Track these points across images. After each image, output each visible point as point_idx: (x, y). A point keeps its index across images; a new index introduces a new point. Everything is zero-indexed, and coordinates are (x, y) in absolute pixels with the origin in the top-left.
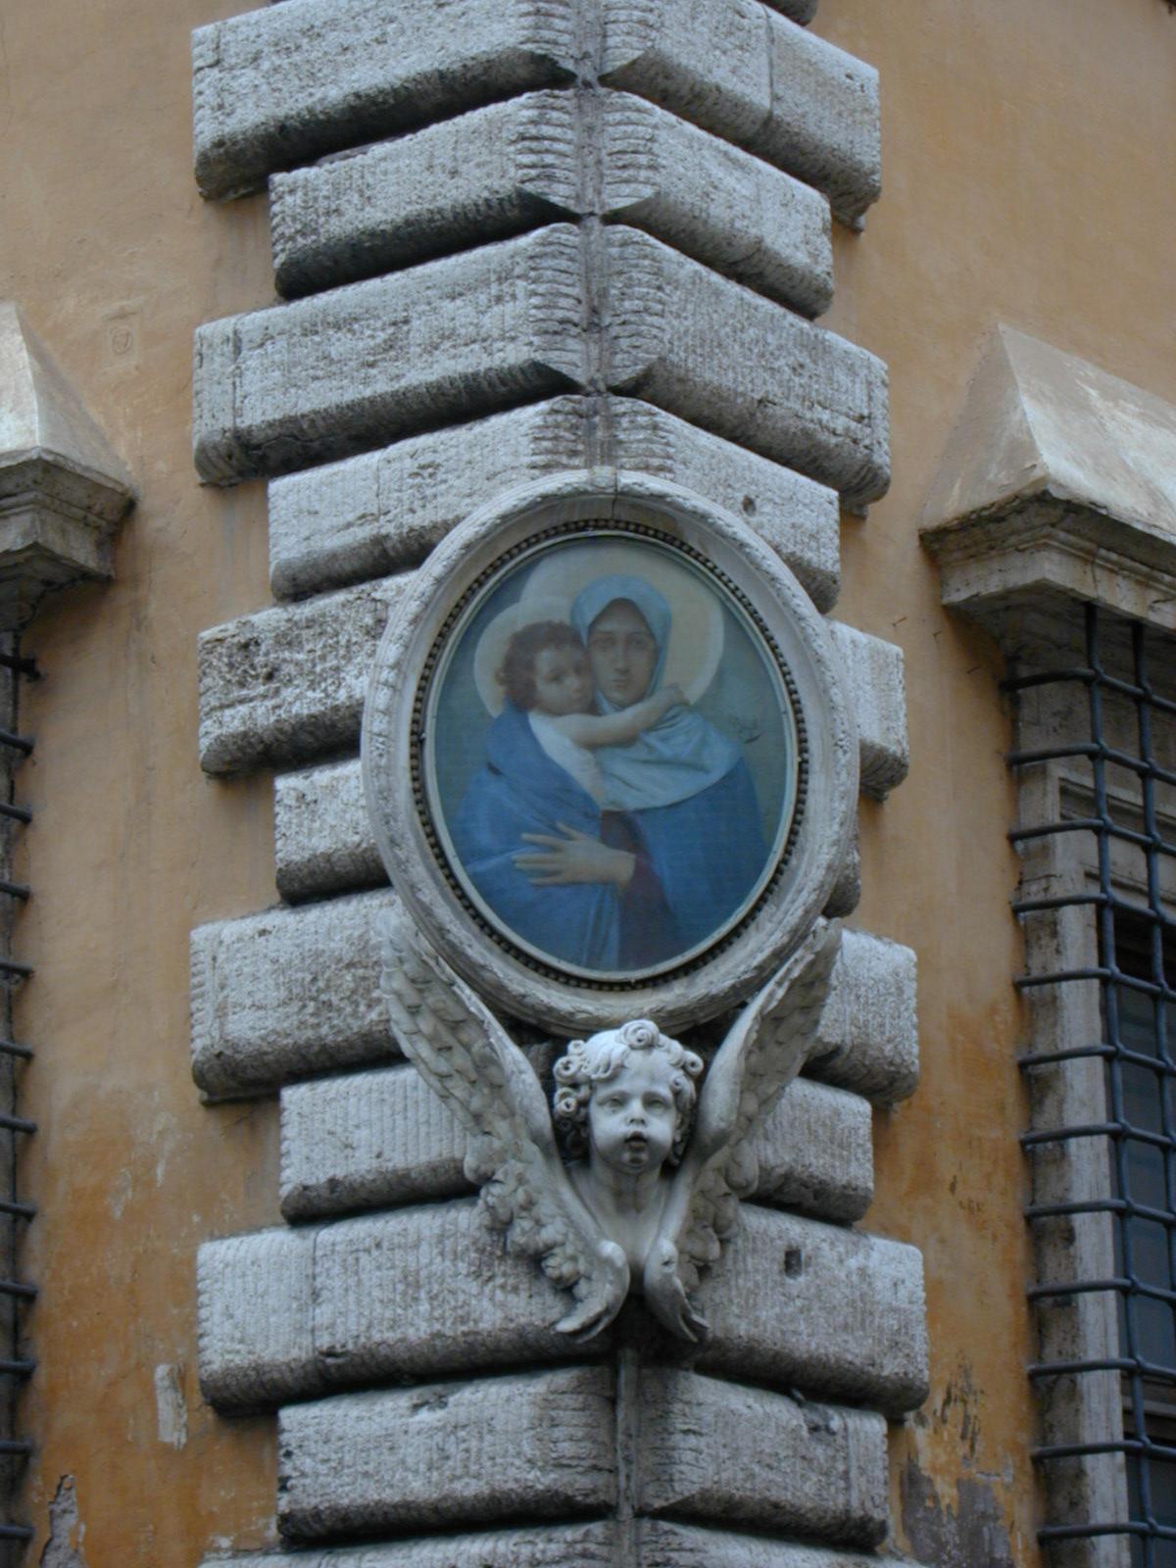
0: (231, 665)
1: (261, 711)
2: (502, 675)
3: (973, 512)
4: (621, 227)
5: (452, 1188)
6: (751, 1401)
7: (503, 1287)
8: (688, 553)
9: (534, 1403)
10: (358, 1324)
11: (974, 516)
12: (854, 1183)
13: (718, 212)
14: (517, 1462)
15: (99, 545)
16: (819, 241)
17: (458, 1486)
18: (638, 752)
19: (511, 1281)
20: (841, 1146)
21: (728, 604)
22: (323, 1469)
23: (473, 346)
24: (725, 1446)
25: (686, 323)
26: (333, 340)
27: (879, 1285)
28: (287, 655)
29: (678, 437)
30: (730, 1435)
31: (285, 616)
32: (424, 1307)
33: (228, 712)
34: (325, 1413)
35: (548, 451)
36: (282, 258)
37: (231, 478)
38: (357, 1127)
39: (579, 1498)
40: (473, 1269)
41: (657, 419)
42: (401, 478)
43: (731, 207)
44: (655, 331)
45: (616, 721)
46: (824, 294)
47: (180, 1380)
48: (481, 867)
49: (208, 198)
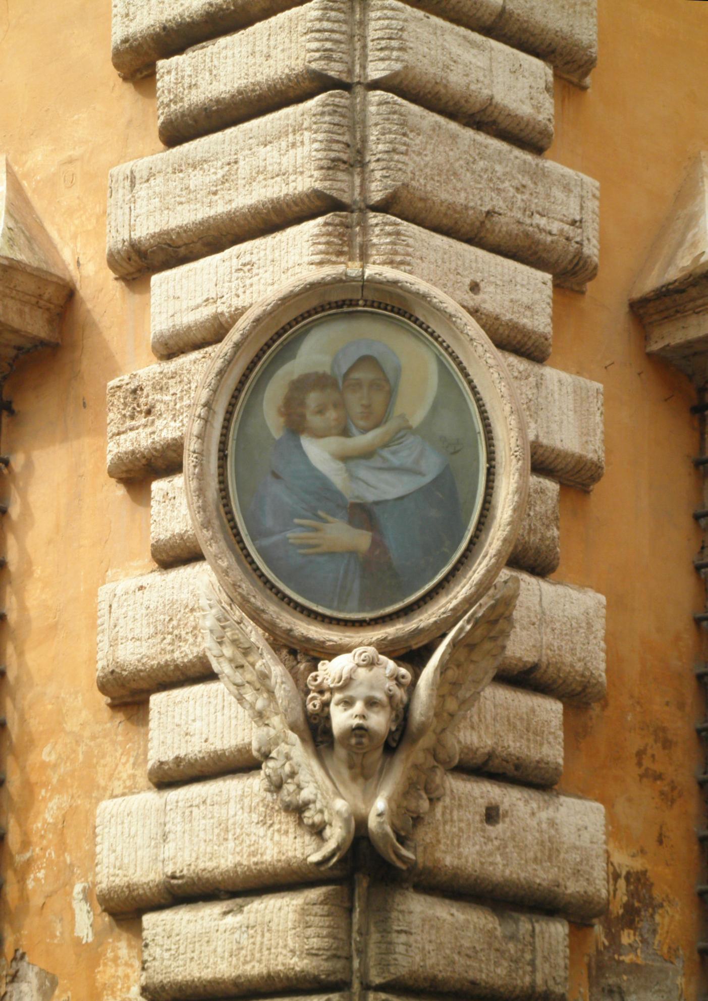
0: (125, 404)
1: (143, 435)
2: (283, 409)
3: (663, 286)
4: (378, 92)
5: (242, 764)
6: (454, 911)
7: (279, 831)
8: (415, 322)
9: (295, 911)
10: (191, 856)
11: (664, 289)
12: (545, 759)
13: (456, 79)
14: (284, 952)
15: (50, 322)
16: (541, 97)
17: (248, 967)
18: (376, 462)
19: (284, 827)
20: (535, 733)
21: (441, 358)
22: (166, 955)
23: (277, 179)
24: (430, 942)
25: (427, 159)
26: (191, 176)
27: (565, 831)
28: (158, 397)
29: (415, 239)
30: (431, 933)
31: (159, 370)
32: (231, 844)
33: (123, 437)
34: (168, 918)
35: (321, 252)
36: (162, 118)
37: (133, 273)
38: (194, 721)
39: (323, 977)
40: (261, 818)
41: (400, 228)
42: (231, 273)
43: (467, 75)
44: (400, 166)
45: (360, 441)
46: (545, 134)
47: (87, 895)
48: (266, 542)
49: (125, 79)
